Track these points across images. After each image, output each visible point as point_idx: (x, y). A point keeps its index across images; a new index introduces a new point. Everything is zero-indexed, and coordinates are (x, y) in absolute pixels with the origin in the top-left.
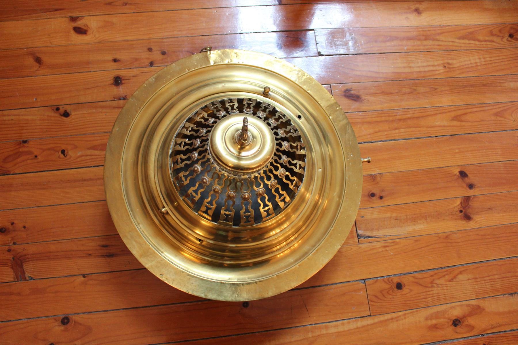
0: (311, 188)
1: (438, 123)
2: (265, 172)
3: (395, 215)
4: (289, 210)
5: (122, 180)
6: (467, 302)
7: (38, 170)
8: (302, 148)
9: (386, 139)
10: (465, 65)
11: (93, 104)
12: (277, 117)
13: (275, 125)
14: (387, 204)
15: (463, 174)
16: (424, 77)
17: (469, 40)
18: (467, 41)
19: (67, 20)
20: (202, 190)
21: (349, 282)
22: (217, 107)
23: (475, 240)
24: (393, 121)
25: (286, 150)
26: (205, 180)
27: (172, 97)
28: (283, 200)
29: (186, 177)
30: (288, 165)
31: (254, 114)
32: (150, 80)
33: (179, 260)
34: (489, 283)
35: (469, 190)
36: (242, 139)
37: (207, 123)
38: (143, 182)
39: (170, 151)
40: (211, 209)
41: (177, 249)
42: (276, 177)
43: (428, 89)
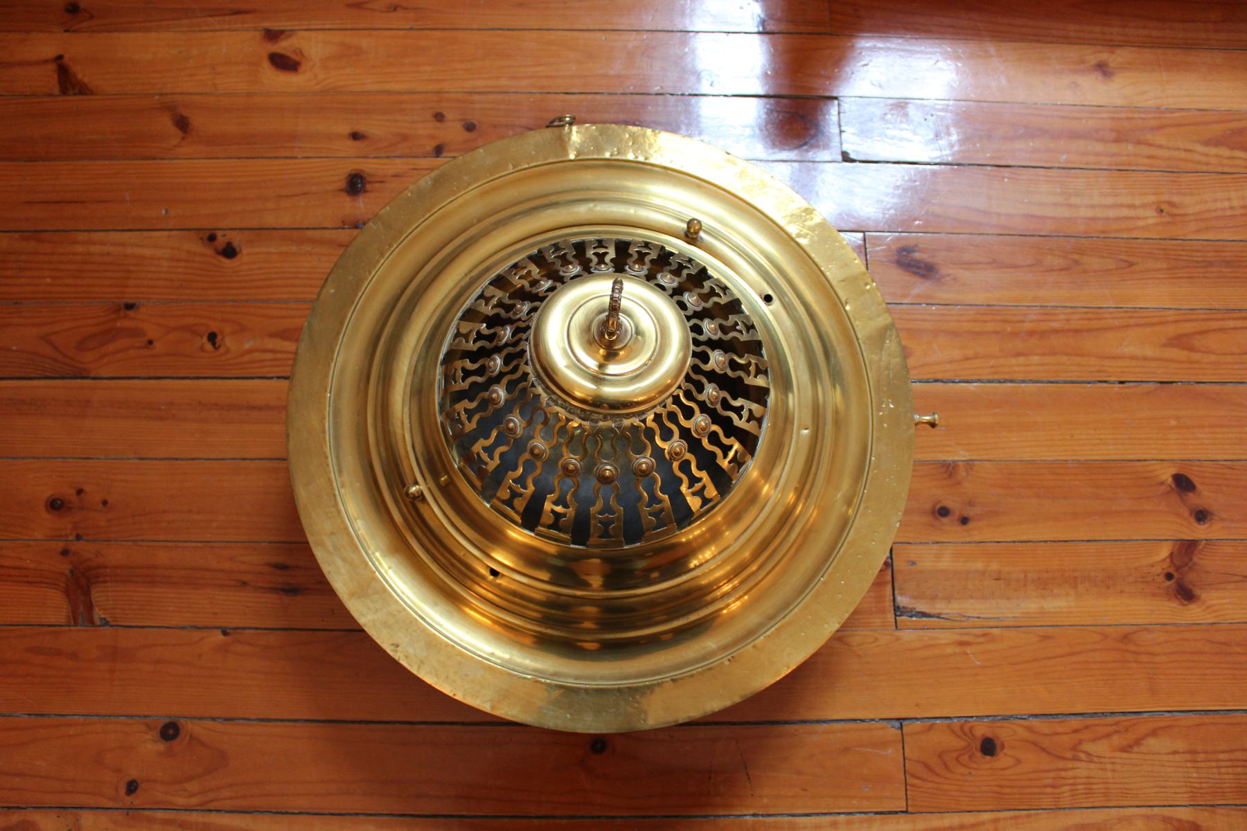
0: (776, 472)
1: (1129, 350)
2: (658, 418)
3: (995, 566)
4: (719, 519)
5: (328, 411)
6: (1166, 812)
7: (152, 375)
8: (759, 372)
9: (991, 377)
10: (1216, 210)
11: (295, 233)
12: (706, 290)
13: (699, 309)
14: (977, 538)
15: (1183, 483)
16: (1103, 232)
17: (1233, 149)
18: (1225, 152)
19: (258, 35)
20: (503, 449)
21: (862, 720)
22: (565, 255)
23: (1202, 653)
24: (1014, 334)
25: (718, 370)
26: (511, 425)
27: (471, 222)
28: (700, 493)
29: (470, 413)
30: (719, 407)
31: (650, 277)
32: (422, 183)
33: (441, 614)
34: (1230, 770)
35: (1196, 524)
36: (607, 334)
37: (534, 291)
38: (375, 419)
39: (444, 349)
40: (521, 495)
41: (453, 600)
42: (685, 434)
43: (1111, 264)
